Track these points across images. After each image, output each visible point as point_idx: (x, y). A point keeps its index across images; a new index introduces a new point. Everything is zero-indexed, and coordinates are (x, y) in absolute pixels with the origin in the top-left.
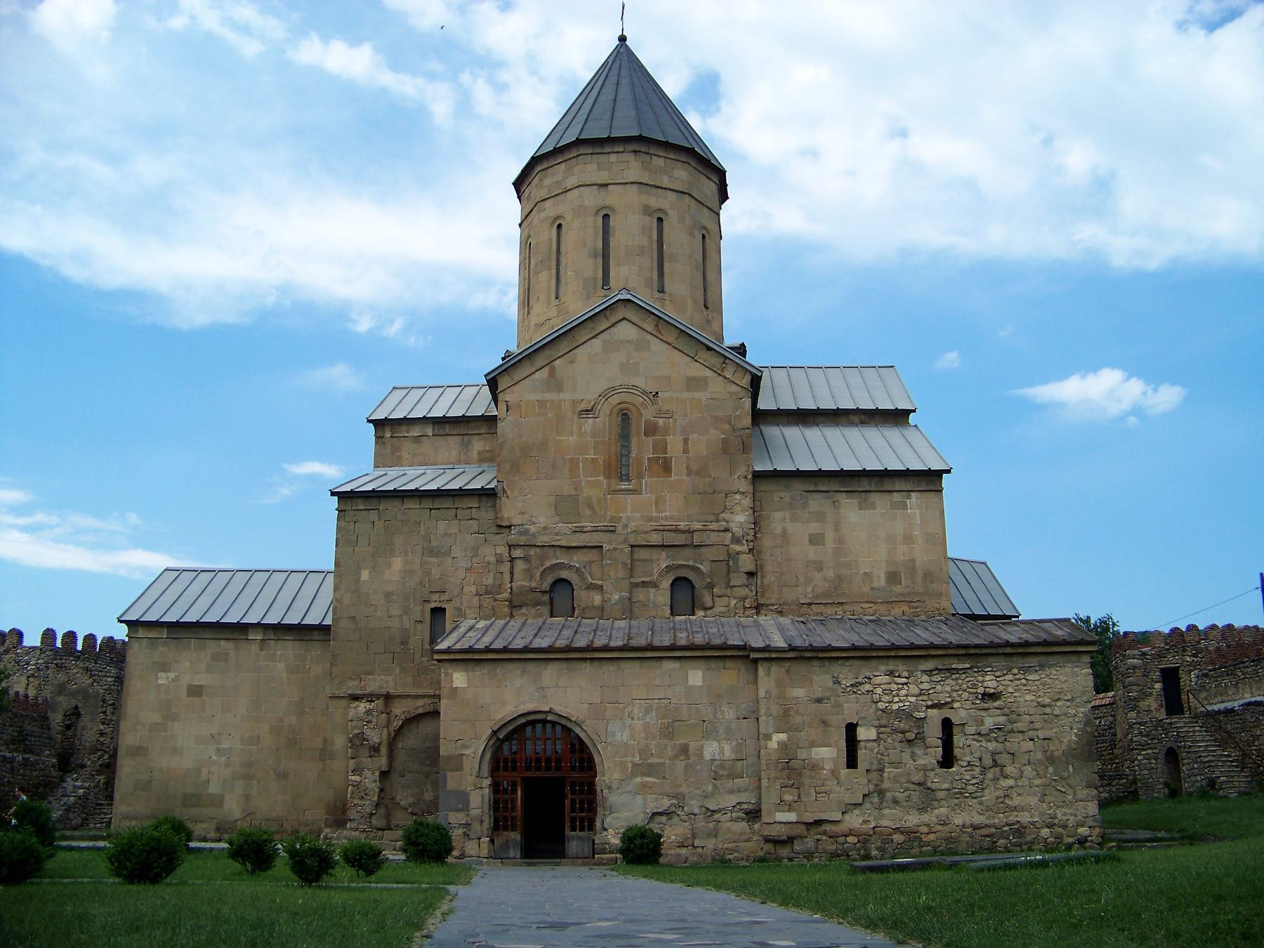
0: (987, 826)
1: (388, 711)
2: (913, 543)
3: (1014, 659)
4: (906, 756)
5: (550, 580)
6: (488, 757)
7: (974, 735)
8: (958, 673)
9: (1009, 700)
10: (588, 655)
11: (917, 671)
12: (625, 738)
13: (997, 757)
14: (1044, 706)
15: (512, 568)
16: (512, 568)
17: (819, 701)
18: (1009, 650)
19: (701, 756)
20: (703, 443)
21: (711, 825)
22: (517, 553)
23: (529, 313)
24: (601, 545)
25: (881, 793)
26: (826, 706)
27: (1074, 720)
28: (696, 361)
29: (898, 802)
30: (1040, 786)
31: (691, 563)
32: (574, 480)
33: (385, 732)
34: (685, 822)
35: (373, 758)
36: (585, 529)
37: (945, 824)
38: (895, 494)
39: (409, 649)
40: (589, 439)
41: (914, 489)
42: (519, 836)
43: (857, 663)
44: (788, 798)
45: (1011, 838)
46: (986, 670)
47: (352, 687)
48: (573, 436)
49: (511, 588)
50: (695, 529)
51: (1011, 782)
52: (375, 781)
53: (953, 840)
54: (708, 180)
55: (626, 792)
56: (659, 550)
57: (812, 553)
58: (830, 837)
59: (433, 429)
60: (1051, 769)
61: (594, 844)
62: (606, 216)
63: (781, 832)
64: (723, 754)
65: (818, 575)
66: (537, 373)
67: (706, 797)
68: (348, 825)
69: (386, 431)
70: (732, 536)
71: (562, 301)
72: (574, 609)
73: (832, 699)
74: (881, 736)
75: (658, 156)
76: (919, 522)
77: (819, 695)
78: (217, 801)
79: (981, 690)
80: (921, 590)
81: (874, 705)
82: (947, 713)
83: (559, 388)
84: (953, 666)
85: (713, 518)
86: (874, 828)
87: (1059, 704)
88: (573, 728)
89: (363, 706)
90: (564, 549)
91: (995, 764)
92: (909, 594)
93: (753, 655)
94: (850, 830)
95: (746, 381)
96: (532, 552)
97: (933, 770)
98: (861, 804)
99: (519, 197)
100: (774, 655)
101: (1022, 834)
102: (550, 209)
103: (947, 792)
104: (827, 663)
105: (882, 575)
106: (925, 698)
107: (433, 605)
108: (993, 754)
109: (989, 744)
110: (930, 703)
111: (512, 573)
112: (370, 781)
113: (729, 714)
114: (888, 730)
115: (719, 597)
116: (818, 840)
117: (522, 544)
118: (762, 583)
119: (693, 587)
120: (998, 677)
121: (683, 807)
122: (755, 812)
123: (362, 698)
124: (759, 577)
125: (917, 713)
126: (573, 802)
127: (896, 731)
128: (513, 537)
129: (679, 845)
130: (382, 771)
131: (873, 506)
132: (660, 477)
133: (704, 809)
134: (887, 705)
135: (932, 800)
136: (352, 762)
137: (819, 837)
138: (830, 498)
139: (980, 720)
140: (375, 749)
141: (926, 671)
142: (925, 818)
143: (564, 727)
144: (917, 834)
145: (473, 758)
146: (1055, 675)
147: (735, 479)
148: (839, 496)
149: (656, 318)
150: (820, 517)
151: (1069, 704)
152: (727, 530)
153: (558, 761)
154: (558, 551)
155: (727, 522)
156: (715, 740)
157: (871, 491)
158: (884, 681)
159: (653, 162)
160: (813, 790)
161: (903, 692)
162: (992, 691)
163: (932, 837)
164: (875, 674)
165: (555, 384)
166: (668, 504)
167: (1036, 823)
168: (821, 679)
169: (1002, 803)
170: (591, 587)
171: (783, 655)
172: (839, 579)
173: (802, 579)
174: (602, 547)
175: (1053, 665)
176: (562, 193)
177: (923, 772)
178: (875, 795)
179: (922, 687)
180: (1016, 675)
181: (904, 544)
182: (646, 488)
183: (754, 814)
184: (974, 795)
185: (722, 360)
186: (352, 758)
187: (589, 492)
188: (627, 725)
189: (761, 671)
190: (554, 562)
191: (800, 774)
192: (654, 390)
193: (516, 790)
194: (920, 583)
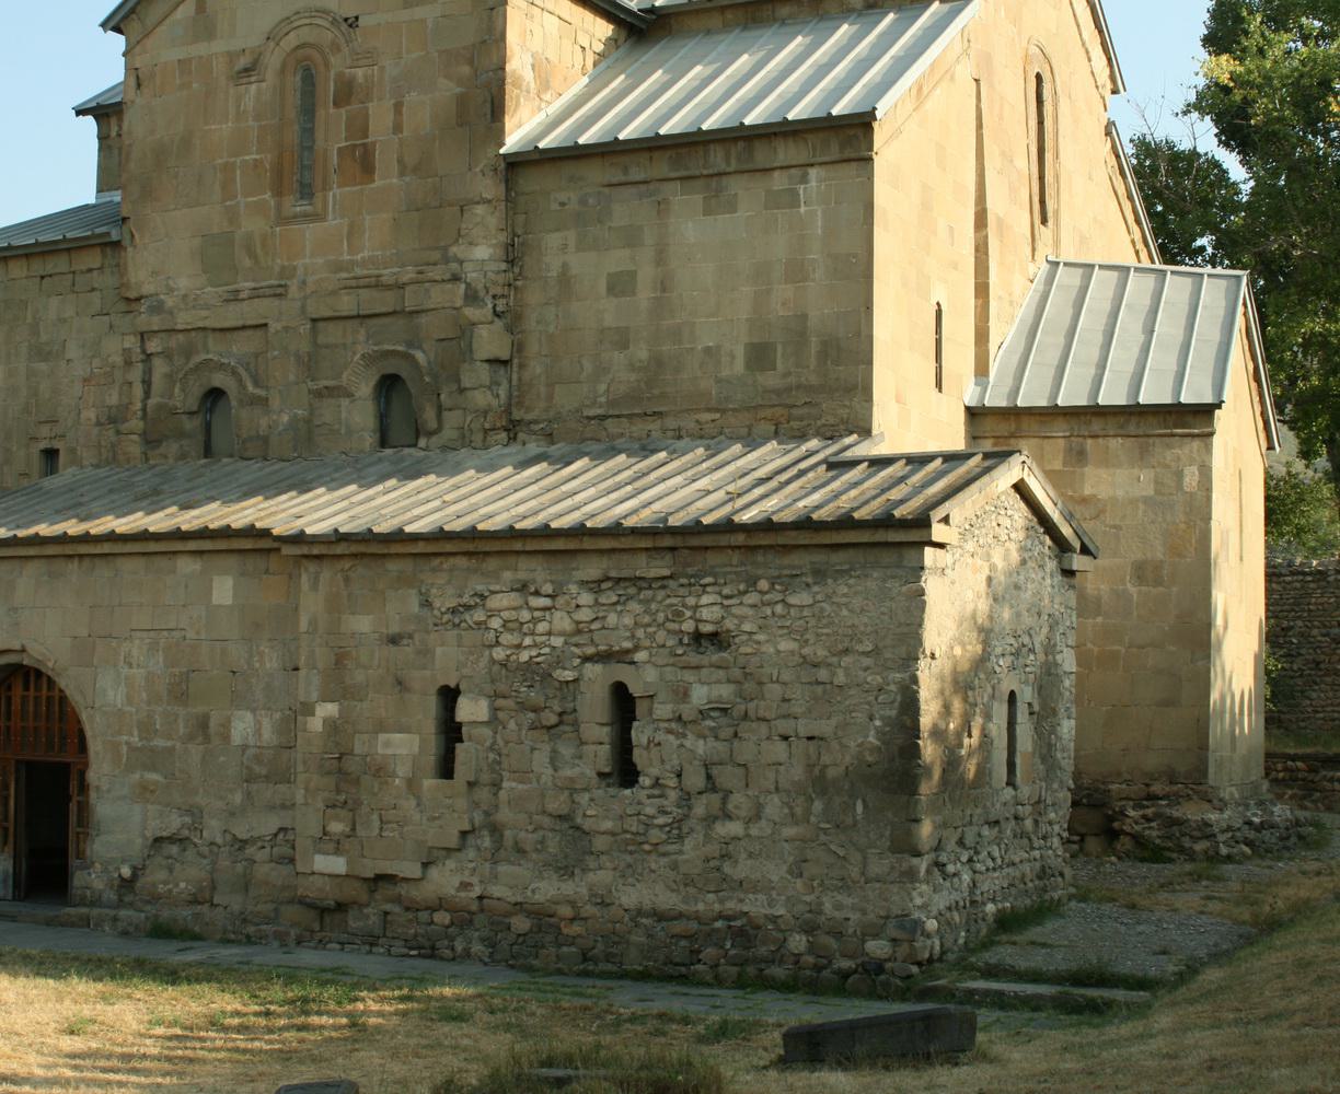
0: (680, 916)
2: (805, 279)
7: (669, 720)
8: (650, 588)
13: (715, 771)
17: (394, 640)
19: (226, 738)
24: (263, 321)
25: (496, 830)
26: (407, 651)
27: (876, 699)
29: (524, 852)
30: (793, 840)
32: (228, 203)
36: (242, 296)
44: (336, 827)
45: (728, 945)
53: (616, 939)
57: (609, 312)
58: (407, 909)
60: (818, 806)
63: (331, 894)
64: (260, 735)
65: (619, 358)
67: (232, 814)
73: (417, 636)
76: (820, 231)
77: (395, 629)
79: (688, 626)
80: (814, 380)
82: (623, 673)
85: (437, 255)
87: (846, 660)
91: (711, 785)
92: (789, 389)
97: (586, 790)
101: (749, 941)
103: (611, 839)
105: (740, 352)
107: (43, 445)
109: (701, 742)
110: (590, 650)
111: (147, 383)
114: (509, 703)
118: (520, 379)
120: (728, 597)
124: (515, 369)
127: (523, 706)
128: (146, 320)
131: (732, 208)
132: (355, 185)
135: (584, 853)
139: (681, 690)
141: (587, 582)
142: (569, 888)
144: (552, 920)
150: (631, 238)
151: (867, 661)
152: (455, 278)
156: (247, 709)
157: (729, 173)
158: (505, 603)
160: (375, 817)
161: (542, 627)
163: (576, 929)
164: (492, 588)
166: (367, 235)
169: (715, 875)
172: (658, 362)
178: (485, 833)
180: (766, 593)
181: (786, 283)
184: (662, 849)
187: (252, 225)
188: (123, 677)
191: (357, 782)
192: (351, 14)
194: (813, 362)
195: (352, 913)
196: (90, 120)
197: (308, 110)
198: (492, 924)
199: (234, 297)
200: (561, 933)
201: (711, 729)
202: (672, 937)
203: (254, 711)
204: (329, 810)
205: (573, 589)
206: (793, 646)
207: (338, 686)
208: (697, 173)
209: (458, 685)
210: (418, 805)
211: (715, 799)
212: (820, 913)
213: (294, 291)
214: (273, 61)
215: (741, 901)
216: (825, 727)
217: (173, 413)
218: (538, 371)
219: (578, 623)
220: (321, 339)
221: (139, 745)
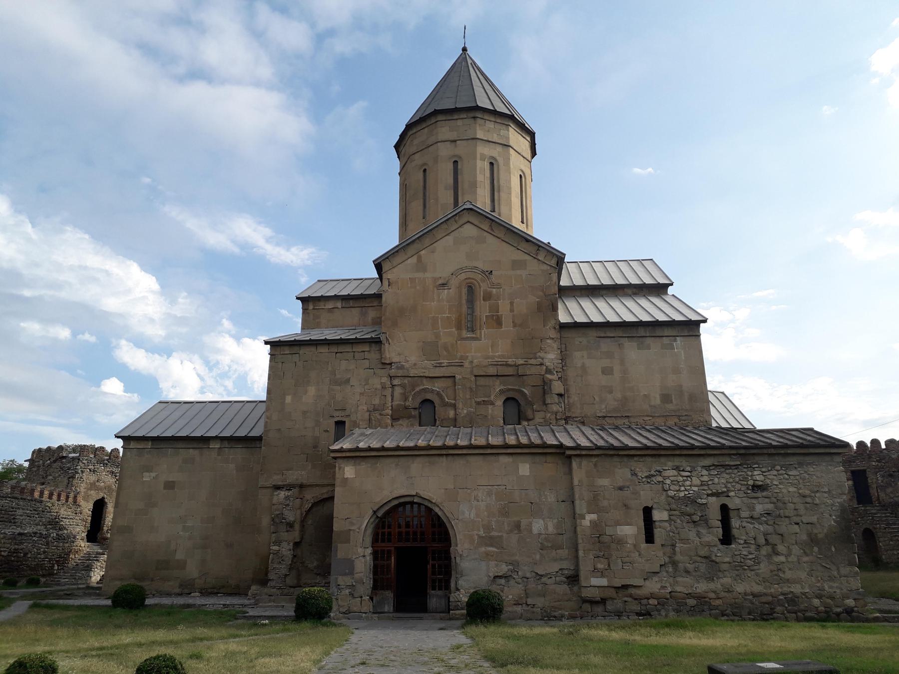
0: (765, 594)
1: (301, 496)
3: (777, 458)
4: (692, 535)
5: (419, 400)
6: (370, 531)
9: (776, 491)
10: (444, 452)
11: (697, 466)
12: (472, 516)
13: (769, 537)
14: (804, 496)
15: (393, 392)
16: (393, 392)
17: (621, 489)
18: (773, 451)
19: (530, 531)
20: (524, 305)
21: (540, 587)
22: (396, 382)
23: (406, 230)
24: (454, 375)
25: (674, 564)
26: (626, 493)
27: (832, 508)
28: (518, 249)
31: (517, 388)
33: (299, 512)
34: (519, 584)
35: (289, 532)
36: (443, 365)
37: (729, 591)
38: (664, 338)
39: (318, 451)
40: (445, 303)
41: (678, 335)
42: (392, 594)
43: (649, 459)
44: (600, 566)
46: (754, 466)
47: (277, 479)
48: (434, 302)
49: (392, 406)
50: (519, 363)
51: (782, 559)
52: (290, 550)
54: (523, 138)
55: (474, 559)
56: (494, 378)
58: (636, 599)
59: (342, 304)
61: (449, 601)
62: (456, 162)
63: (595, 594)
64: (547, 530)
66: (409, 260)
68: (269, 584)
69: (310, 305)
70: (546, 369)
71: (427, 220)
72: (435, 420)
74: (672, 517)
75: (490, 121)
76: (683, 358)
78: (182, 565)
79: (751, 482)
81: (665, 493)
83: (424, 270)
84: (727, 463)
86: (670, 592)
87: (817, 495)
88: (433, 508)
89: (282, 494)
90: (428, 379)
91: (767, 542)
93: (568, 452)
94: (651, 594)
95: (553, 262)
96: (406, 381)
97: (715, 546)
98: (658, 573)
99: (398, 157)
100: (584, 453)
102: (418, 159)
103: (729, 565)
104: (625, 459)
105: (658, 397)
106: (706, 488)
107: (337, 419)
108: (765, 534)
110: (710, 492)
111: (392, 396)
112: (286, 550)
113: (551, 498)
114: (677, 513)
115: (538, 411)
116: (626, 601)
117: (400, 375)
118: (568, 402)
119: (519, 405)
120: (765, 472)
121: (518, 572)
122: (574, 577)
123: (283, 488)
124: (566, 398)
125: (699, 500)
126: (434, 566)
127: (683, 514)
128: (393, 372)
129: (514, 602)
130: (295, 542)
131: (649, 348)
133: (534, 574)
134: (675, 493)
136: (274, 535)
137: (626, 599)
138: (617, 342)
140: (290, 525)
142: (712, 586)
143: (426, 507)
144: (706, 599)
145: (358, 532)
146: (812, 471)
147: (547, 329)
148: (622, 340)
149: (490, 221)
150: (609, 355)
151: (826, 495)
152: (541, 364)
153: (422, 533)
154: (425, 380)
155: (543, 359)
158: (671, 474)
159: (486, 125)
160: (619, 560)
161: (688, 483)
162: (761, 483)
163: (718, 602)
164: (665, 468)
165: (421, 266)
167: (807, 594)
168: (622, 473)
170: (446, 405)
171: (591, 453)
173: (597, 399)
174: (454, 377)
175: (810, 464)
176: (426, 148)
177: (707, 547)
179: (702, 479)
180: (779, 471)
182: (485, 336)
183: (573, 579)
184: (752, 568)
185: (537, 247)
186: (274, 533)
189: (575, 464)
190: (422, 387)
193: (391, 557)
195: (608, 603)
196: (299, 301)
197: (471, 301)
198: (678, 603)
199: (440, 366)
200: (711, 605)
201: (765, 521)
202: (761, 603)
203: (543, 519)
204: (595, 559)
205: (699, 469)
206: (795, 489)
207: (594, 505)
208: (635, 335)
209: (652, 506)
210: (639, 555)
211: (769, 548)
212: (824, 590)
213: (467, 364)
214: (454, 282)
215: (790, 587)
216: (814, 519)
217: (406, 408)
218: (576, 399)
219: (702, 481)
220: (478, 383)
221: (484, 535)
